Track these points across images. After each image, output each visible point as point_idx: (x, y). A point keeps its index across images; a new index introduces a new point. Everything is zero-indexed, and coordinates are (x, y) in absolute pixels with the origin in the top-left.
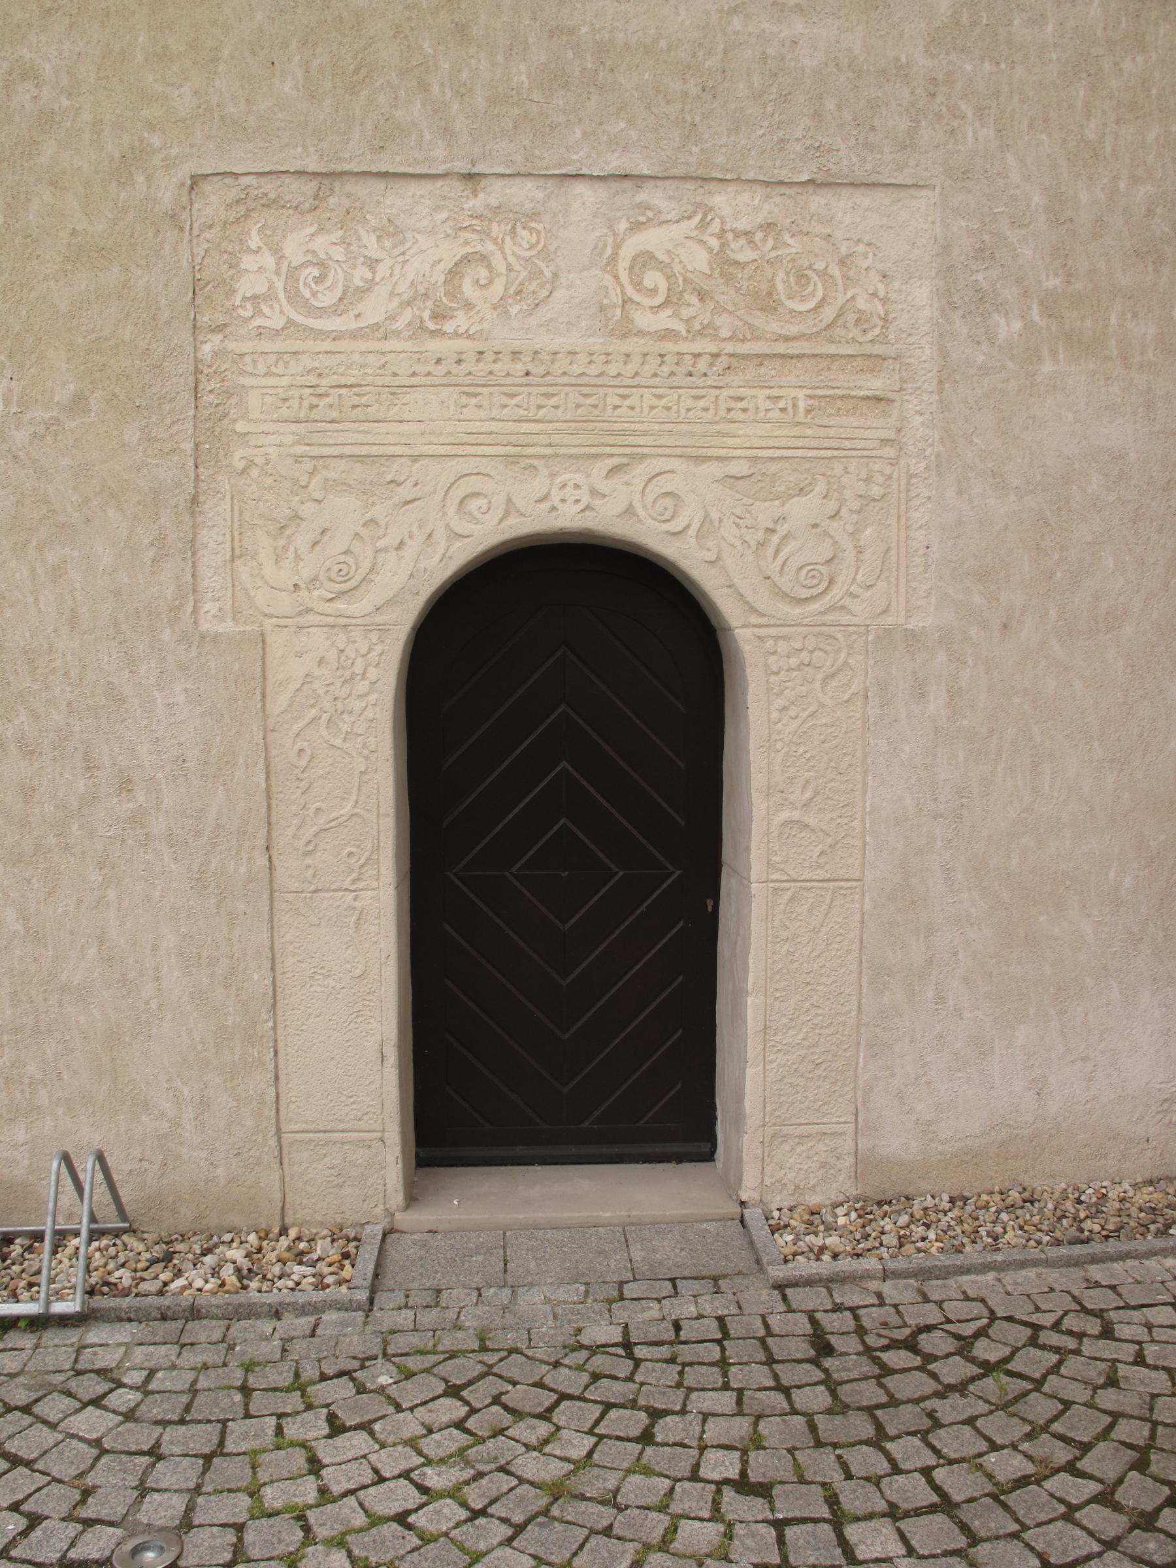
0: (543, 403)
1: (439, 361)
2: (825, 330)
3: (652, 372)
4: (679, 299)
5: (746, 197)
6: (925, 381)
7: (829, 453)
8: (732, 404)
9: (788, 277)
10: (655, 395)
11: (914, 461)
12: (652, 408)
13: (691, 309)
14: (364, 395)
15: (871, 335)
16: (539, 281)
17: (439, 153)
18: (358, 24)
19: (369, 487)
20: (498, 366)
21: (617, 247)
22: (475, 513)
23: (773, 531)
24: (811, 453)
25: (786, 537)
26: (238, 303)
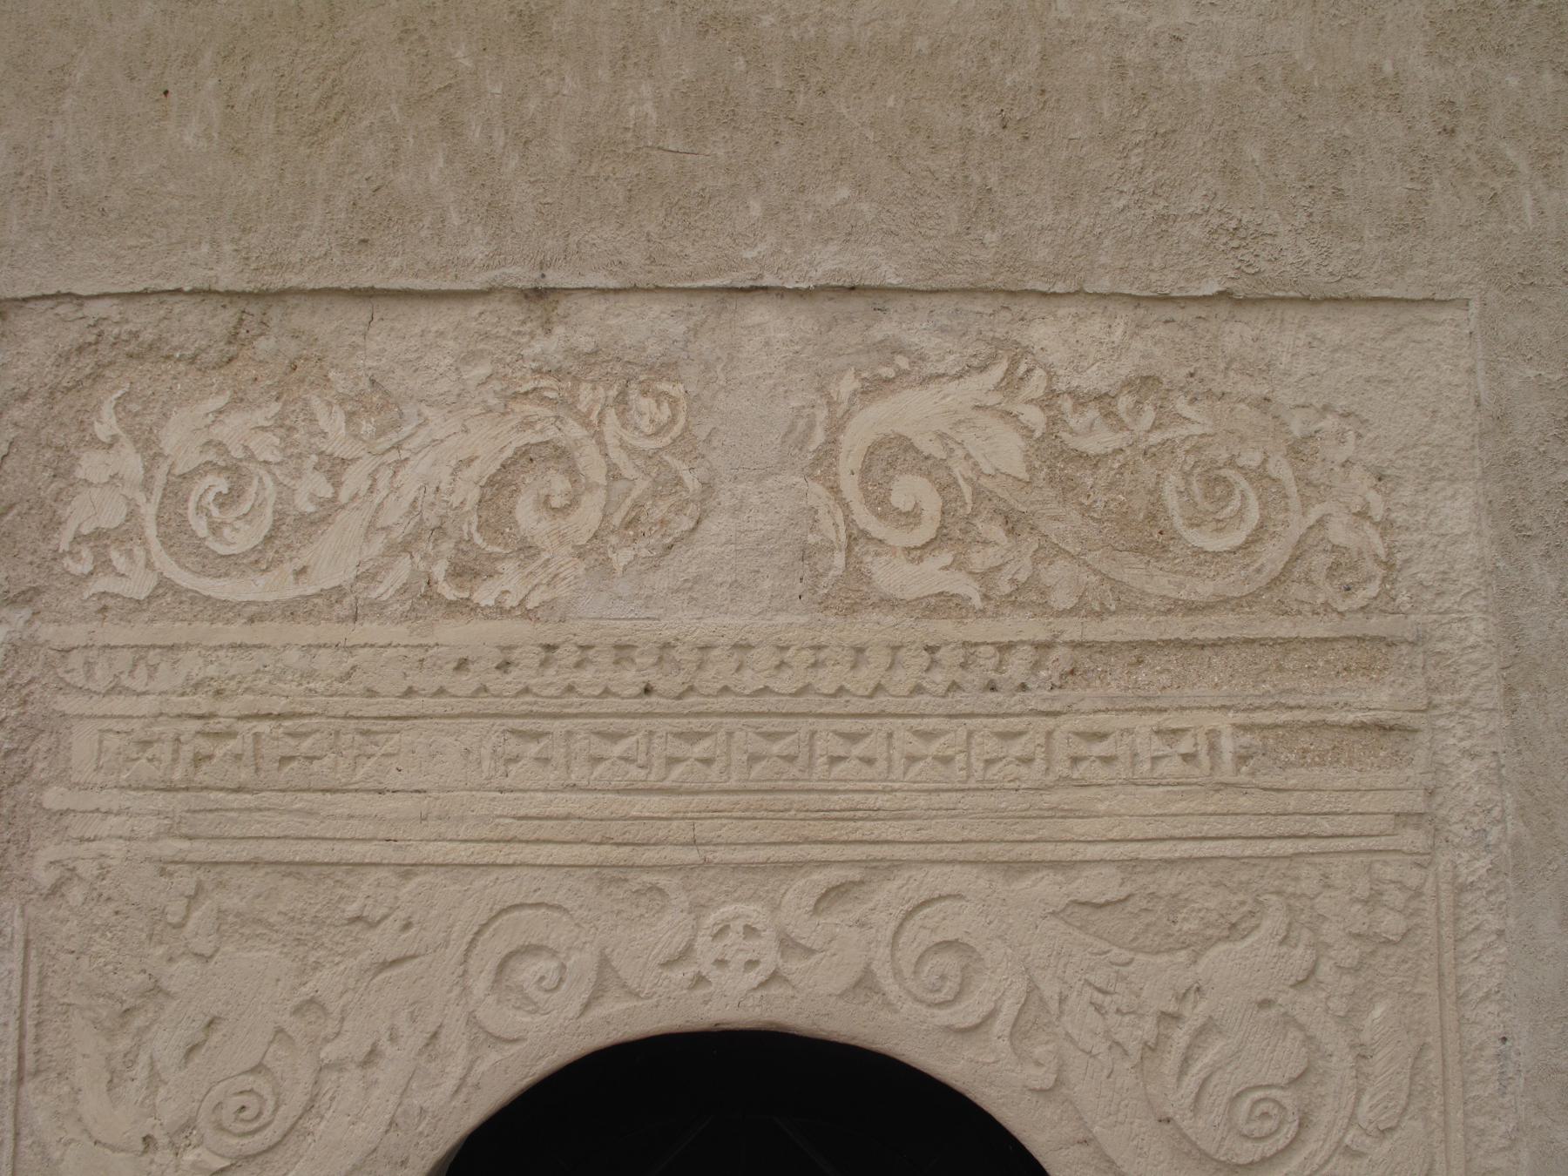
0: (679, 754)
1: (462, 665)
2: (1268, 588)
3: (912, 683)
4: (965, 532)
5: (1096, 326)
6: (1476, 688)
7: (1288, 847)
8: (1082, 748)
9: (1188, 483)
10: (916, 733)
11: (1466, 856)
12: (912, 759)
13: (990, 550)
14: (306, 735)
15: (1360, 597)
16: (672, 499)
17: (477, 250)
18: (332, 19)
19: (310, 929)
20: (587, 675)
21: (836, 428)
22: (532, 990)
23: (1176, 1018)
24: (1258, 848)
25: (1203, 1032)
26: (64, 547)
